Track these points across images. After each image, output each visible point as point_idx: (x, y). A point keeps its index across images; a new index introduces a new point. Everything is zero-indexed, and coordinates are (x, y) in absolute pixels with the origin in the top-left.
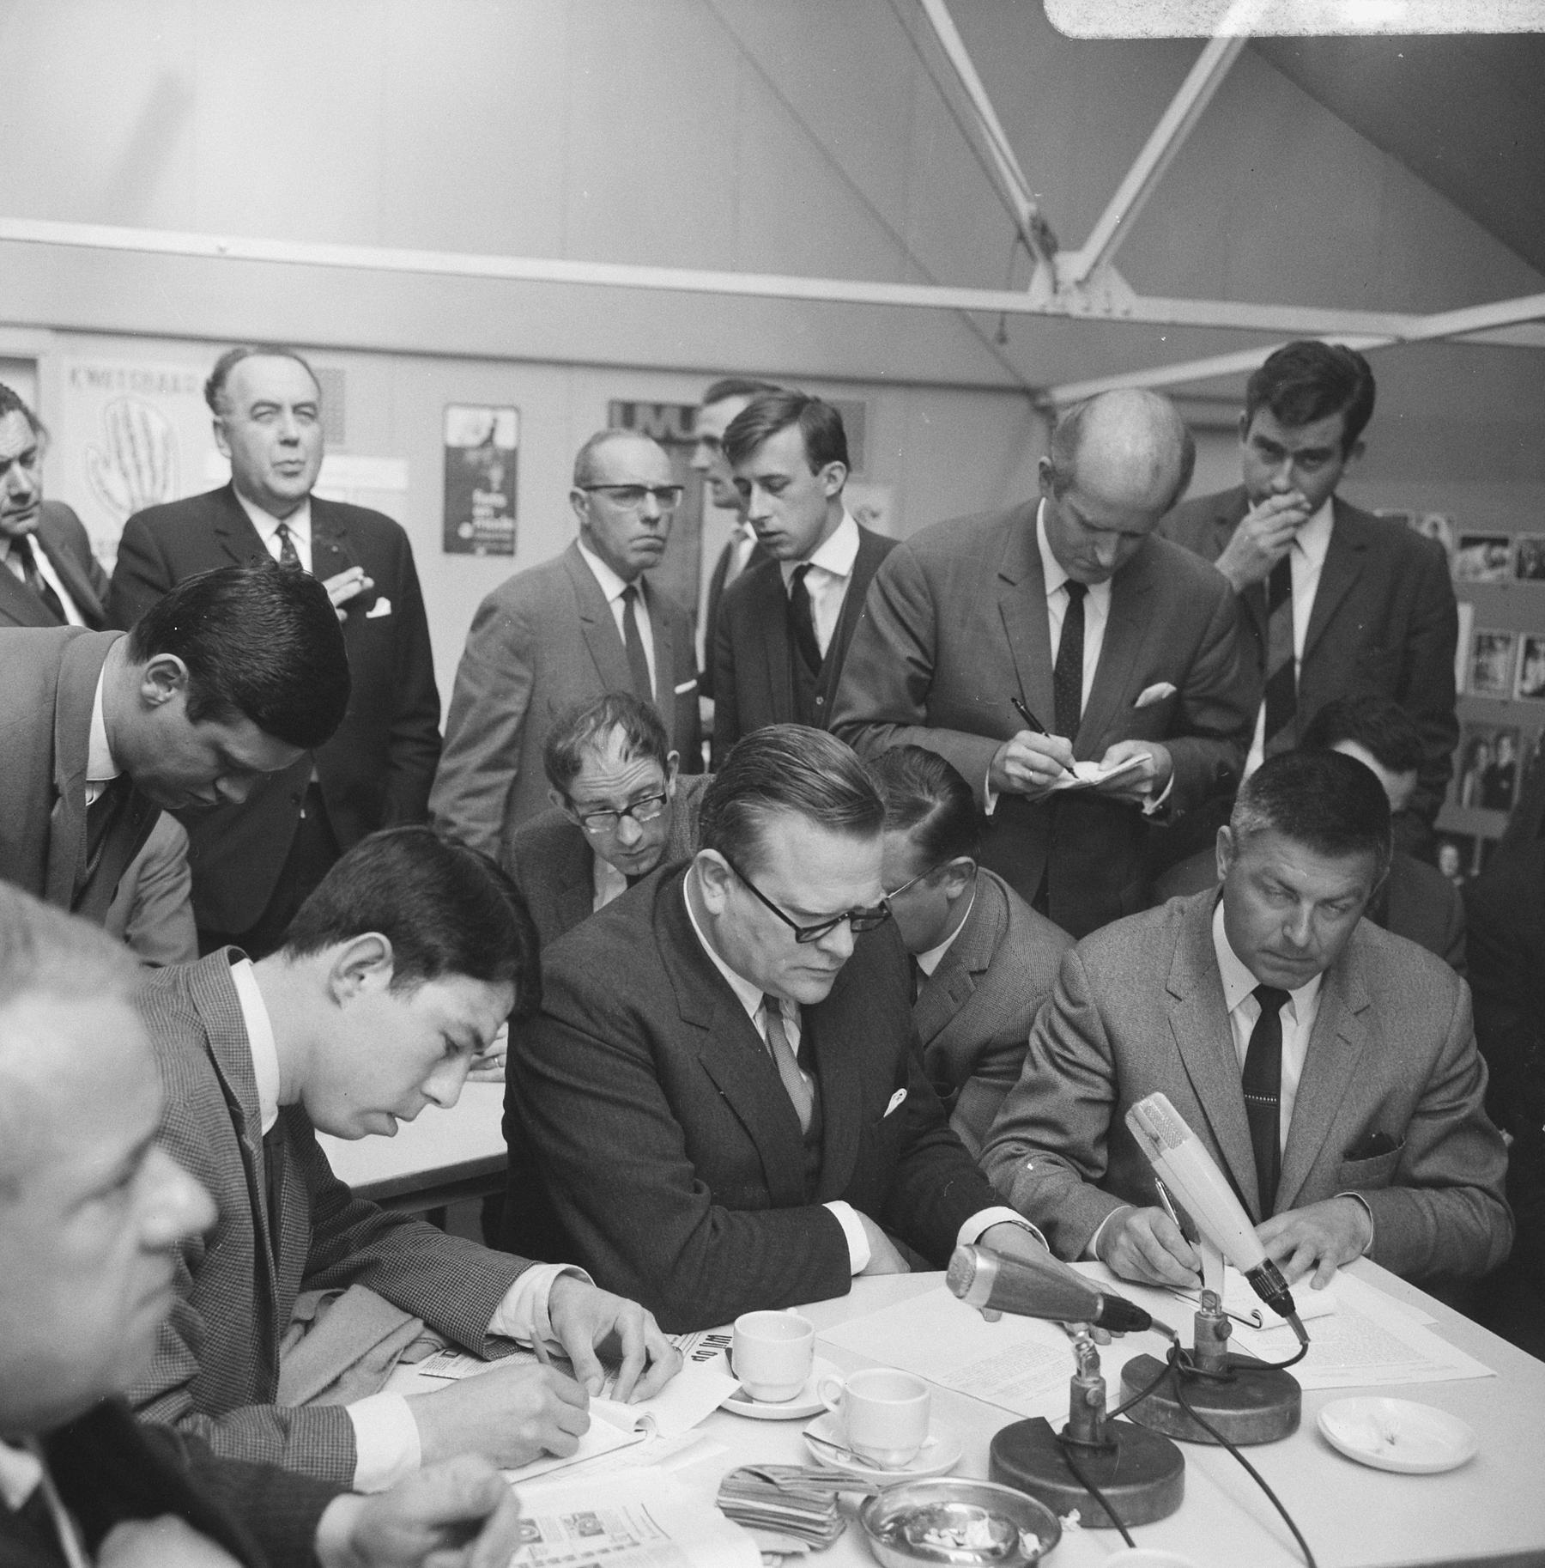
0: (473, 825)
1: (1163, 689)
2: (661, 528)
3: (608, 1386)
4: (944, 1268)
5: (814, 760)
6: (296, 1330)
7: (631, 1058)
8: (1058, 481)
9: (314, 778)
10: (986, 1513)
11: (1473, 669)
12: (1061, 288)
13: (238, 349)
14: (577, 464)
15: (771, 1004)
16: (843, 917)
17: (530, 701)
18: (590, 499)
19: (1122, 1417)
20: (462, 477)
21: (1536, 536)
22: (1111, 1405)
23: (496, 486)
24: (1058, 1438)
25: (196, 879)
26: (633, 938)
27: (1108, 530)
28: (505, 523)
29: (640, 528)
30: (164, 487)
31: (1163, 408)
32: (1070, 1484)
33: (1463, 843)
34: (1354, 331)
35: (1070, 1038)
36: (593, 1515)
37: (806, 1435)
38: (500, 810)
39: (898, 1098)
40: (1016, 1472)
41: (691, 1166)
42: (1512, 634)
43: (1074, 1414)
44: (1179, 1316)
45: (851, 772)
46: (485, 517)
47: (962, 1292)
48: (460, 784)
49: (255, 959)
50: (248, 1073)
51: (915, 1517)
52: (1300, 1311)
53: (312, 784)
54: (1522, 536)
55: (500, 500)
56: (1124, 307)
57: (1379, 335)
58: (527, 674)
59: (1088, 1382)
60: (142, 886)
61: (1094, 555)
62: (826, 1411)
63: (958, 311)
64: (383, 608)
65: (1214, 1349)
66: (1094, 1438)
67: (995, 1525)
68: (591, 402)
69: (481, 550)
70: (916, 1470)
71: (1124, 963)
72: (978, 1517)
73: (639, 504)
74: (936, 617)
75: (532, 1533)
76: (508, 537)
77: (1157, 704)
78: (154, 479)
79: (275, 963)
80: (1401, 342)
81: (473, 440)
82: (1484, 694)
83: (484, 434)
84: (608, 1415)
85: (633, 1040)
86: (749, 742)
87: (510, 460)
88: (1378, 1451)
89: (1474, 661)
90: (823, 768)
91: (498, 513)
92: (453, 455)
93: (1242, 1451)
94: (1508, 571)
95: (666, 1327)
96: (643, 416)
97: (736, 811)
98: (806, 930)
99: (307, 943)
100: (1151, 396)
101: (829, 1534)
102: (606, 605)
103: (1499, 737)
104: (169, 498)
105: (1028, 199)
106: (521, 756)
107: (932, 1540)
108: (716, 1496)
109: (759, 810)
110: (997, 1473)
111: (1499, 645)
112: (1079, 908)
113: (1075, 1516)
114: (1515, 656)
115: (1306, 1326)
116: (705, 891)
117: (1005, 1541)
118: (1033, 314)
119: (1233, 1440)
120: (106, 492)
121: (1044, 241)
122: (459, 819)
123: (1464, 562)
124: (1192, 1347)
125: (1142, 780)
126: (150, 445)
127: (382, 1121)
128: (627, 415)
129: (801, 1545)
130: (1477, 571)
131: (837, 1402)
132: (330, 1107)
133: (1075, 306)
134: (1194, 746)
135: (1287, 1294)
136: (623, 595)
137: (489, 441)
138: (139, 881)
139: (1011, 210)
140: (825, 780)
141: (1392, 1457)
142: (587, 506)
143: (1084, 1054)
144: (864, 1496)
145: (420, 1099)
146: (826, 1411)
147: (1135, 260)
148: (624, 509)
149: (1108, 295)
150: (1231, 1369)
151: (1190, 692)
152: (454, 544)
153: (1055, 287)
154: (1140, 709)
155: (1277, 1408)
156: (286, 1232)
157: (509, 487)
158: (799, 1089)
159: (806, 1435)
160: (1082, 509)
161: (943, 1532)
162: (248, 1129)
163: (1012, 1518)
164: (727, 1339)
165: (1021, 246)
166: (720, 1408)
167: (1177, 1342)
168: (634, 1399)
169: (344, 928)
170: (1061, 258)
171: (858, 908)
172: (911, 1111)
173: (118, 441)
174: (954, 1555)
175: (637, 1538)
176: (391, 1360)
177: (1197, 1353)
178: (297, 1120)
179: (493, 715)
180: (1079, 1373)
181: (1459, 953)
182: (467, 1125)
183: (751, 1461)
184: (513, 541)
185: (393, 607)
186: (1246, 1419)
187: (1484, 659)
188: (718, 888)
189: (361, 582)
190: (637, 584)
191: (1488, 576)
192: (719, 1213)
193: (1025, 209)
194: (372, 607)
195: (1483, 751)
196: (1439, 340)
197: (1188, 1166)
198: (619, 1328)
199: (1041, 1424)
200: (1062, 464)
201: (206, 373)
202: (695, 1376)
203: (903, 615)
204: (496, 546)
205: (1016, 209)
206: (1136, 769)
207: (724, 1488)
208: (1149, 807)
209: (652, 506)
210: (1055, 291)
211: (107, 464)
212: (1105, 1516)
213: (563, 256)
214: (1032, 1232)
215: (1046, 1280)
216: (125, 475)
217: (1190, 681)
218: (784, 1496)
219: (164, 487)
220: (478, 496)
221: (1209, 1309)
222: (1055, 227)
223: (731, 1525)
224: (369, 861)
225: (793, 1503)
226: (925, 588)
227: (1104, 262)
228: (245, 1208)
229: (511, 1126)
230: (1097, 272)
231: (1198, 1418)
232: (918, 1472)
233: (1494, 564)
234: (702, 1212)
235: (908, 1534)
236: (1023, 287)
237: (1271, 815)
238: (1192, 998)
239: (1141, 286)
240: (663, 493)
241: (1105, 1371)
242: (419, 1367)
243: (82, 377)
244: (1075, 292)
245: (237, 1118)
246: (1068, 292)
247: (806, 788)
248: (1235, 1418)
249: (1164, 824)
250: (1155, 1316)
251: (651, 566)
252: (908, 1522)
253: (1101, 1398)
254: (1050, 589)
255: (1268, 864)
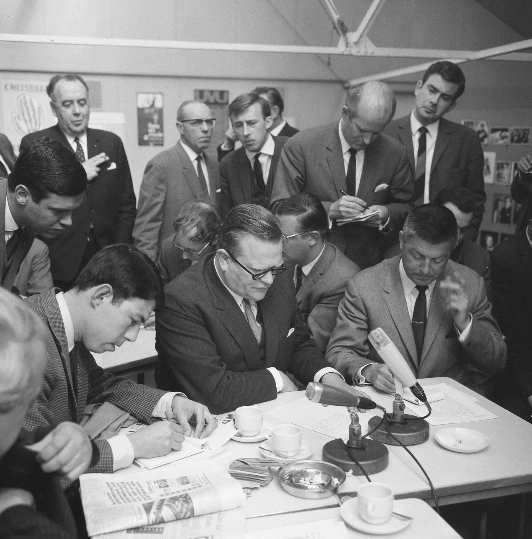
0: (148, 241)
1: (384, 186)
2: (209, 134)
3: (193, 433)
4: (305, 389)
5: (256, 216)
6: (86, 418)
7: (197, 322)
8: (350, 114)
9: (92, 226)
10: (320, 472)
11: (496, 175)
12: (349, 45)
13: (57, 77)
14: (178, 113)
15: (246, 302)
16: (269, 270)
17: (166, 198)
18: (183, 125)
19: (368, 437)
20: (144, 118)
21: (518, 127)
22: (363, 434)
23: (156, 121)
24: (346, 446)
25: (52, 263)
26: (196, 280)
27: (368, 131)
28: (160, 135)
29: (201, 135)
30: (40, 125)
31: (385, 88)
32: (349, 461)
33: (494, 235)
34: (456, 57)
35: (352, 309)
36: (186, 477)
37: (260, 447)
38: (157, 235)
39: (292, 331)
40: (331, 457)
41: (219, 357)
42: (510, 163)
43: (350, 437)
44: (387, 403)
45: (269, 220)
46: (153, 133)
47: (311, 398)
48: (143, 227)
49: (65, 292)
50: (62, 331)
51: (296, 474)
52: (429, 399)
53: (91, 229)
54: (512, 128)
55: (157, 126)
56: (371, 51)
57: (461, 59)
58: (164, 188)
59: (355, 427)
60: (33, 266)
61: (363, 140)
62: (267, 439)
63: (317, 54)
64: (113, 166)
65: (399, 413)
66: (357, 445)
67: (324, 476)
68: (187, 91)
69: (152, 144)
70: (297, 458)
71: (368, 284)
72: (318, 473)
73: (200, 126)
74: (305, 163)
75: (165, 484)
76: (161, 139)
77: (382, 191)
78: (36, 122)
79: (72, 293)
80: (469, 61)
81: (147, 105)
82: (500, 183)
83: (151, 103)
84: (191, 443)
85: (197, 316)
86: (233, 211)
87: (160, 112)
88: (455, 446)
89: (497, 172)
90: (259, 219)
91: (157, 131)
92: (140, 111)
93: (407, 447)
94: (508, 140)
95: (212, 412)
96: (207, 95)
97: (230, 235)
98: (256, 275)
99: (83, 287)
100: (382, 84)
101: (267, 481)
102: (190, 162)
103: (506, 198)
104: (41, 128)
105: (337, 14)
106: (163, 217)
107: (302, 482)
108: (228, 469)
109: (238, 234)
110: (325, 458)
111: (505, 166)
112: (364, 260)
113: (351, 471)
114: (511, 170)
115: (431, 405)
116: (221, 263)
117: (327, 481)
118: (339, 55)
119: (404, 443)
120: (19, 128)
121: (343, 28)
122: (142, 239)
123: (493, 138)
124: (392, 413)
125: (378, 219)
126: (34, 111)
127: (110, 347)
128: (200, 95)
129: (257, 485)
130: (497, 141)
131: (270, 436)
132: (91, 343)
133: (354, 51)
134: (396, 206)
135: (424, 394)
136: (197, 159)
137: (153, 106)
138: (32, 264)
139: (331, 18)
140: (260, 223)
141: (460, 447)
142: (182, 128)
143: (357, 314)
144: (279, 468)
145: (123, 339)
146: (267, 439)
147: (375, 34)
148: (195, 128)
149: (366, 47)
150: (405, 420)
151: (393, 187)
152: (142, 142)
153: (347, 45)
154: (377, 193)
155: (420, 432)
156: (79, 387)
157: (160, 121)
158: (257, 329)
159: (260, 447)
160: (359, 124)
161: (306, 479)
162: (63, 350)
163: (330, 473)
164: (234, 416)
165: (335, 31)
166: (231, 439)
167: (385, 412)
168: (201, 437)
169: (96, 281)
170: (349, 34)
171: (274, 267)
172: (297, 335)
173: (22, 110)
174: (309, 487)
175: (200, 484)
176: (118, 427)
177: (394, 415)
178: (81, 346)
179: (154, 202)
180: (352, 423)
181: (488, 275)
182: (143, 345)
183: (240, 457)
184: (163, 141)
185: (117, 166)
186: (409, 436)
187: (500, 171)
188: (225, 261)
189: (105, 158)
190: (201, 155)
191: (501, 142)
192: (230, 373)
193: (336, 17)
194: (109, 166)
195: (500, 203)
196: (482, 59)
197: (391, 353)
198: (195, 413)
199: (340, 441)
200: (352, 108)
201: (47, 83)
202: (223, 428)
203: (294, 163)
204: (156, 143)
205: (333, 18)
206: (376, 215)
207: (231, 467)
208: (381, 228)
209: (205, 126)
210: (347, 46)
211: (19, 118)
212: (361, 471)
213: (176, 39)
214: (340, 375)
215: (340, 393)
216: (26, 121)
217: (393, 183)
218: (251, 469)
219: (40, 125)
220: (150, 125)
221: (398, 400)
222: (347, 24)
223: (233, 479)
224: (106, 256)
225: (251, 470)
226: (300, 152)
227: (364, 35)
228: (63, 377)
229: (158, 347)
230: (361, 39)
231: (393, 437)
232: (298, 458)
233: (503, 138)
234: (223, 373)
235: (294, 480)
236: (336, 45)
237: (415, 230)
238: (393, 293)
239: (378, 44)
240: (209, 122)
241: (361, 422)
242: (129, 429)
243: (9, 87)
244: (354, 46)
245: (59, 347)
246: (351, 46)
247: (254, 226)
248: (406, 436)
249: (386, 233)
250: (378, 403)
251: (206, 148)
252: (294, 476)
253: (360, 432)
254: (344, 152)
255: (414, 247)
